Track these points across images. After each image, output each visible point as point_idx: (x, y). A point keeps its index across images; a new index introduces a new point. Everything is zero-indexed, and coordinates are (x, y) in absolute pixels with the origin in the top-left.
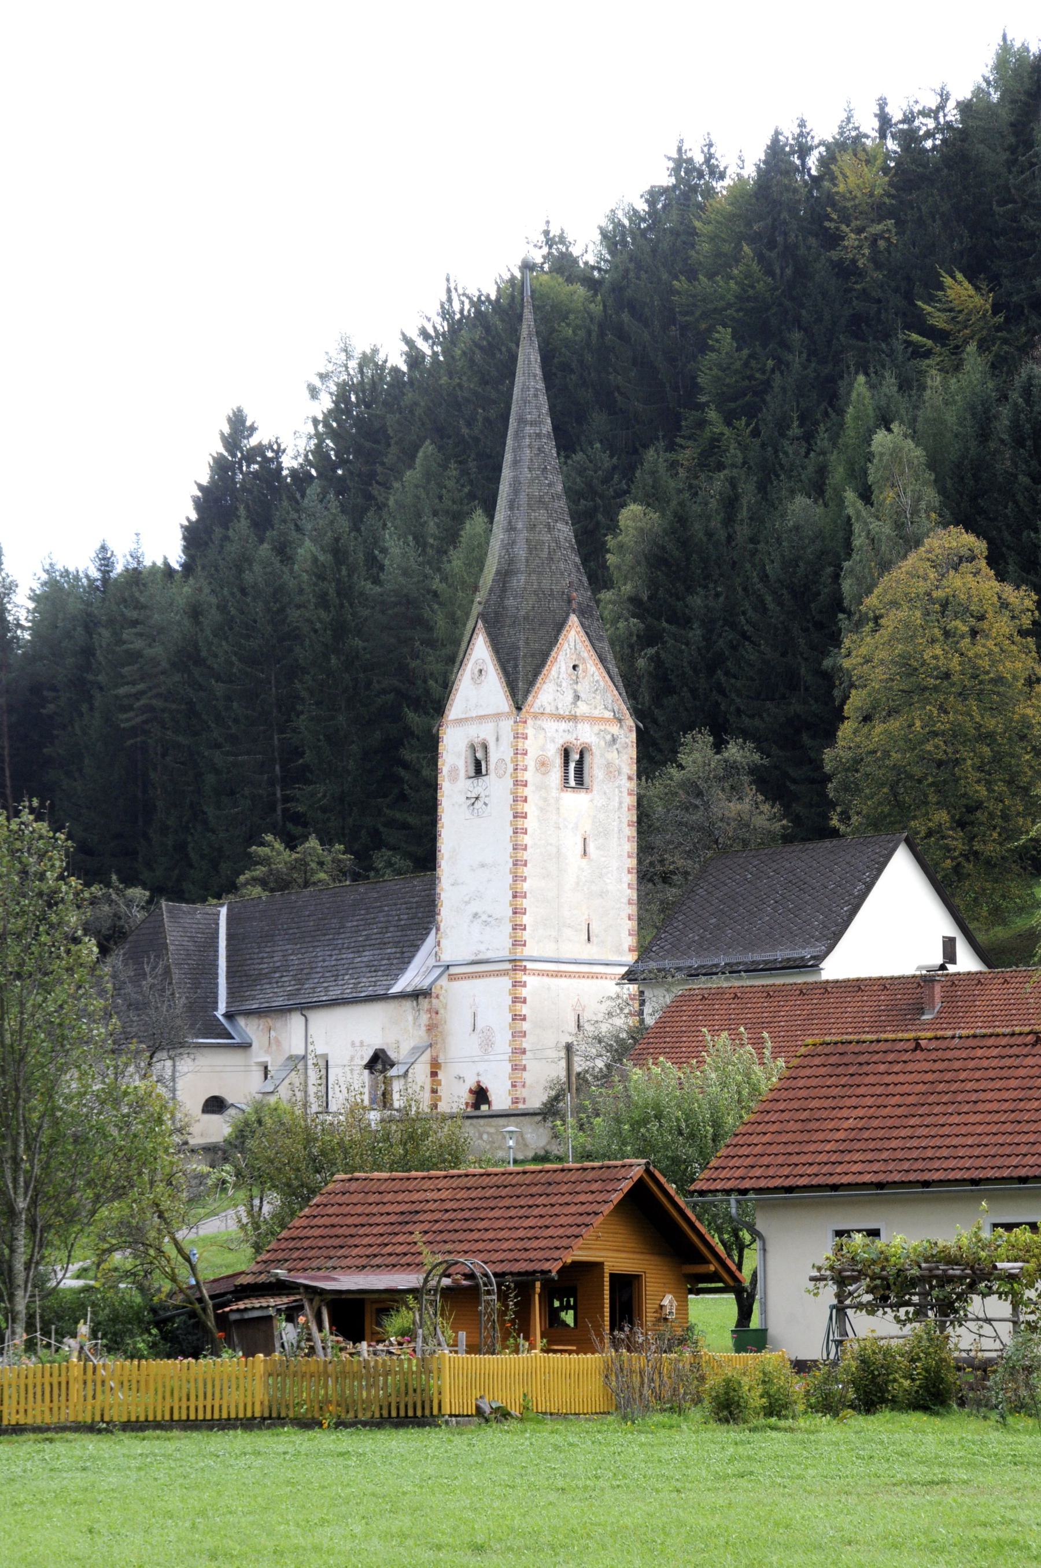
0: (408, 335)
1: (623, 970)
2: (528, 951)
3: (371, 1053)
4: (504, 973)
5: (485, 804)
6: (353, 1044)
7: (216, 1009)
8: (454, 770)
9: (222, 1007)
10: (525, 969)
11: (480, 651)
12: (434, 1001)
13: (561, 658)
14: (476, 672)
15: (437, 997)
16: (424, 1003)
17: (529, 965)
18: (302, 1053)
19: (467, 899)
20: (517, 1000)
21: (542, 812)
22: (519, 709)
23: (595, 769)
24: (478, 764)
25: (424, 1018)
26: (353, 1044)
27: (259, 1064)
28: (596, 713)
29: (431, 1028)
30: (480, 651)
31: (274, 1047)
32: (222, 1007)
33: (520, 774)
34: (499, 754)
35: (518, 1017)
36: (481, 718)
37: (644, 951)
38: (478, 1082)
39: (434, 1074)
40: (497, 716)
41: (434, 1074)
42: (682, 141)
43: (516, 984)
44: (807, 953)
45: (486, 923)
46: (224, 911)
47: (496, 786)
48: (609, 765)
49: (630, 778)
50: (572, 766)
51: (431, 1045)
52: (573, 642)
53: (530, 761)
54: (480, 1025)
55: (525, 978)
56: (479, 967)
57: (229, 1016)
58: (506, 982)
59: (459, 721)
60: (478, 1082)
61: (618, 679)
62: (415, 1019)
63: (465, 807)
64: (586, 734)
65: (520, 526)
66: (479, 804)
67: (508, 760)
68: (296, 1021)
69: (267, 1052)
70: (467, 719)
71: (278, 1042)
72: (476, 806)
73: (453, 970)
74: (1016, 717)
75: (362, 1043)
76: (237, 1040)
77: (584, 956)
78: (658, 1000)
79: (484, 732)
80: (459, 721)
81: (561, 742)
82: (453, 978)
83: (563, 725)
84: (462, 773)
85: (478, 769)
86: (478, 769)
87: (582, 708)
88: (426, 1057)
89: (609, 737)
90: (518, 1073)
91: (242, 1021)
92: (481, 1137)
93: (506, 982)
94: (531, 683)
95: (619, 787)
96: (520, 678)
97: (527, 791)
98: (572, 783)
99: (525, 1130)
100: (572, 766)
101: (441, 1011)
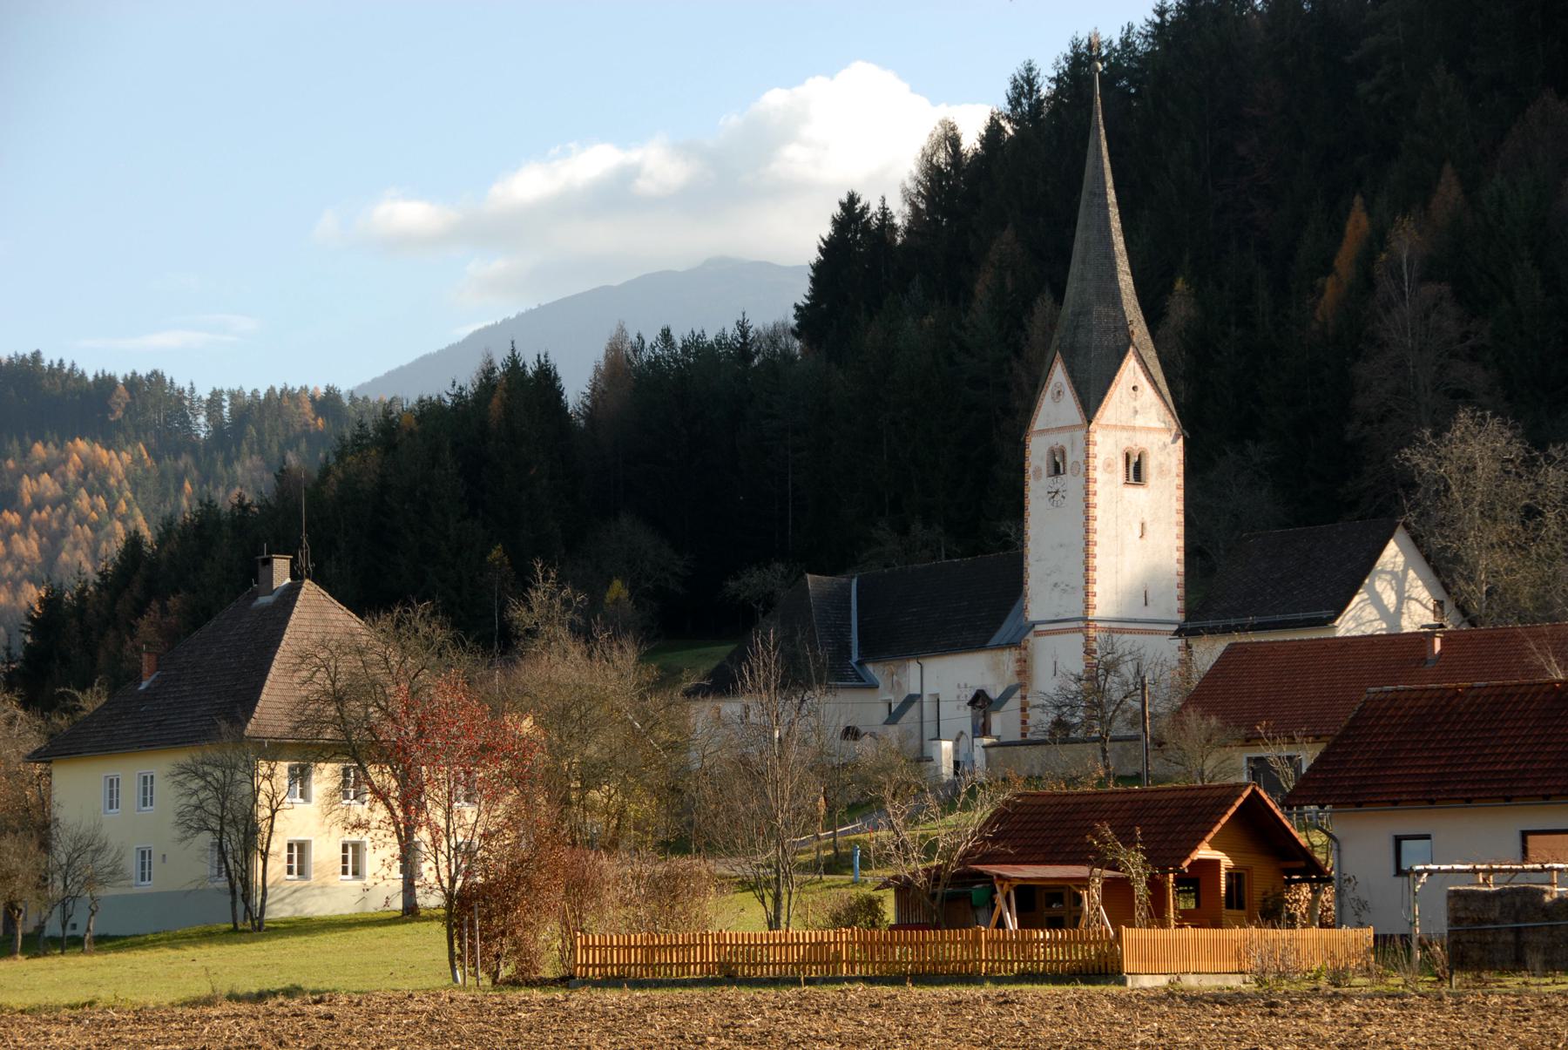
0: (888, 204)
1: (1175, 628)
7: (850, 657)
8: (1038, 471)
9: (855, 657)
11: (1058, 375)
21: (1118, 501)
23: (1151, 467)
24: (1057, 466)
30: (1058, 375)
36: (1059, 429)
37: (1191, 611)
40: (1072, 428)
42: (884, 199)
44: (1325, 614)
45: (1064, 591)
46: (855, 581)
47: (1069, 481)
48: (1161, 465)
52: (1130, 371)
57: (860, 664)
58: (1080, 638)
59: (1042, 432)
61: (1169, 398)
64: (1140, 442)
65: (1090, 276)
66: (1058, 497)
71: (899, 684)
73: (1039, 628)
74: (93, 1040)
78: (1208, 652)
79: (1061, 439)
80: (1042, 432)
82: (1038, 634)
83: (1125, 434)
85: (1057, 470)
86: (1057, 470)
87: (1139, 421)
94: (1100, 402)
96: (1091, 397)
98: (1132, 480)
100: (239, 900)
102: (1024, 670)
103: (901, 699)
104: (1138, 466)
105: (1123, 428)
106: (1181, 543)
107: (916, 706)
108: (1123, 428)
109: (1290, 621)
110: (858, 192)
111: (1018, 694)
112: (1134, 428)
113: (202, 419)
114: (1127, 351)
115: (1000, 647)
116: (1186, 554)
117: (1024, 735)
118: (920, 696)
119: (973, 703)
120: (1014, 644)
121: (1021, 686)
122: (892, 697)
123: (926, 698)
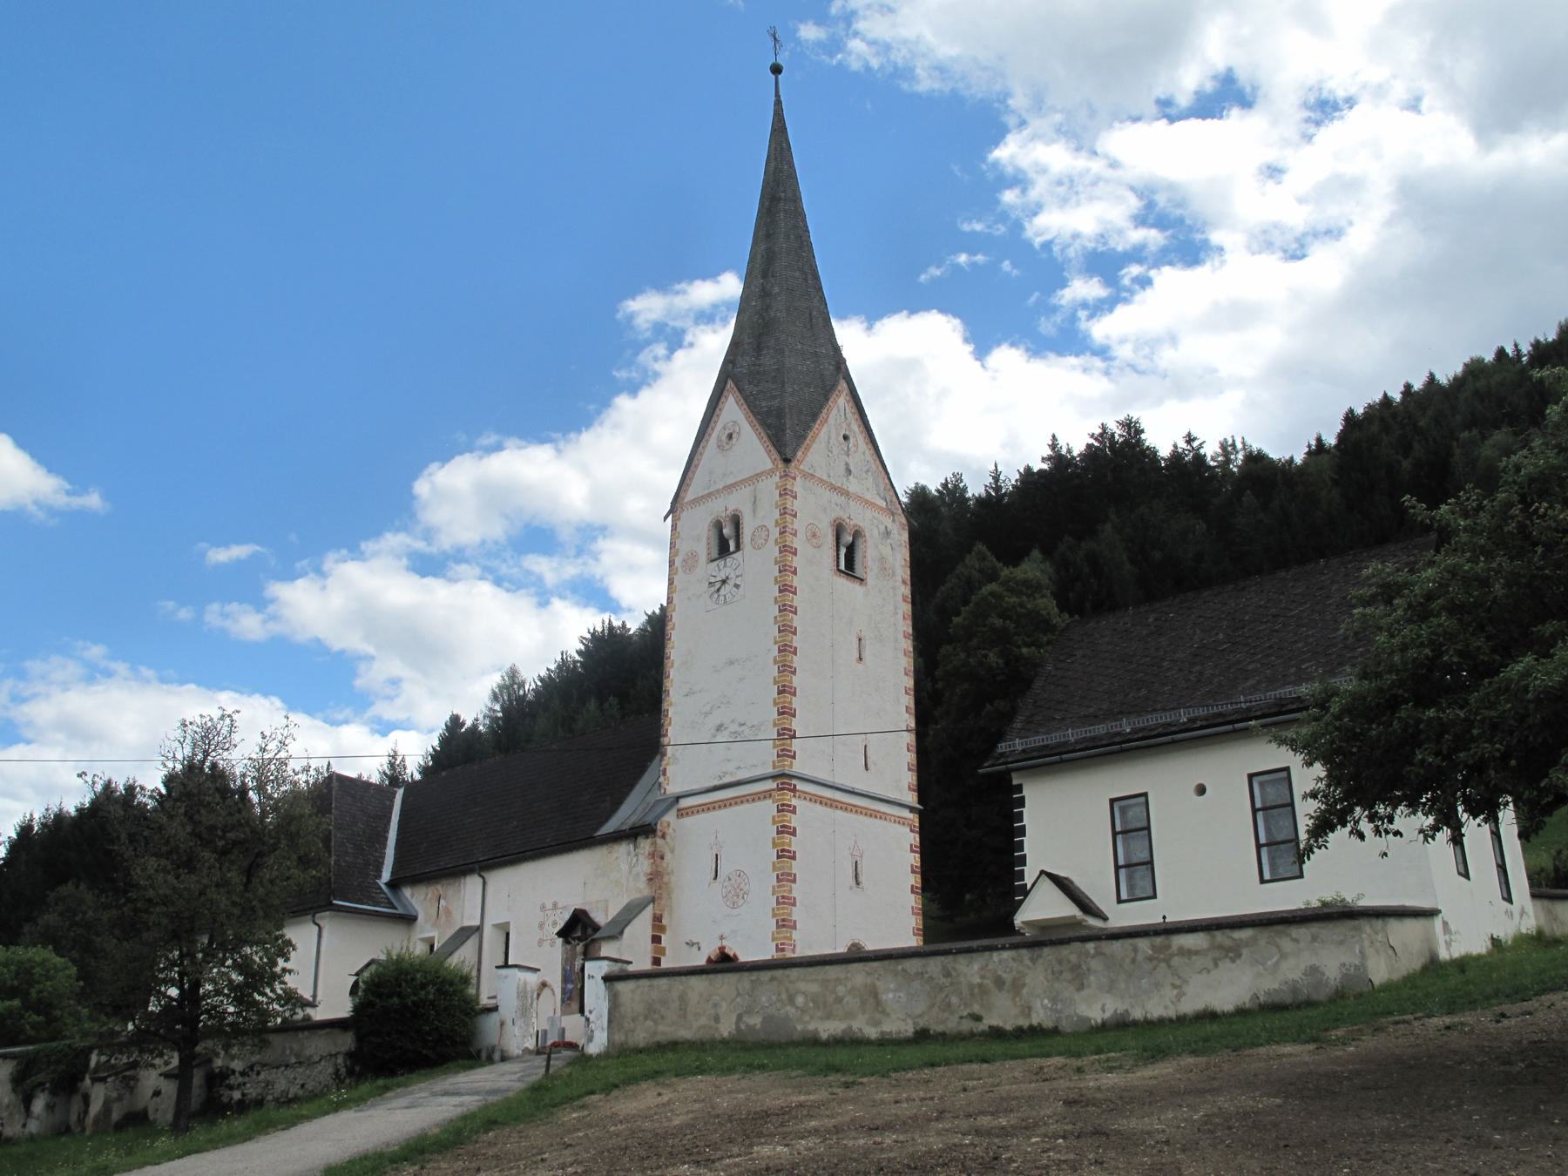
2: (797, 767)
3: (567, 916)
4: (766, 795)
5: (737, 586)
6: (543, 907)
7: (379, 877)
10: (794, 790)
12: (659, 841)
13: (831, 420)
14: (724, 438)
15: (663, 836)
16: (645, 844)
17: (800, 786)
18: (477, 923)
19: (707, 708)
20: (785, 830)
22: (787, 461)
23: (869, 555)
25: (645, 866)
26: (543, 907)
27: (422, 940)
28: (868, 496)
29: (655, 877)
31: (443, 917)
32: (386, 875)
33: (789, 539)
34: (759, 519)
35: (785, 854)
36: (729, 488)
38: (722, 949)
39: (656, 939)
41: (656, 939)
43: (783, 808)
49: (904, 582)
50: (843, 551)
51: (653, 900)
53: (798, 524)
54: (722, 873)
55: (794, 802)
56: (725, 792)
57: (391, 885)
58: (769, 807)
60: (722, 949)
62: (865, 18)
63: (707, 596)
67: (771, 525)
68: (472, 884)
69: (434, 925)
70: (710, 495)
71: (448, 912)
72: (722, 592)
75: (555, 905)
76: (400, 911)
77: (860, 786)
81: (834, 516)
82: (682, 813)
84: (703, 558)
88: (648, 913)
89: (882, 528)
90: (785, 932)
91: (407, 892)
92: (791, 1000)
93: (769, 807)
95: (894, 588)
97: (796, 562)
99: (880, 985)
101: (668, 856)
102: (655, 897)
103: (450, 932)
104: (851, 550)
105: (833, 488)
106: (910, 683)
107: (471, 944)
108: (833, 488)
109: (1045, 751)
110: (1149, 292)
111: (648, 913)
112: (846, 494)
113: (978, 227)
114: (833, 387)
115: (617, 837)
116: (918, 702)
117: (657, 961)
118: (479, 929)
119: (565, 933)
120: (642, 831)
121: (653, 900)
122: (434, 933)
123: (488, 931)
